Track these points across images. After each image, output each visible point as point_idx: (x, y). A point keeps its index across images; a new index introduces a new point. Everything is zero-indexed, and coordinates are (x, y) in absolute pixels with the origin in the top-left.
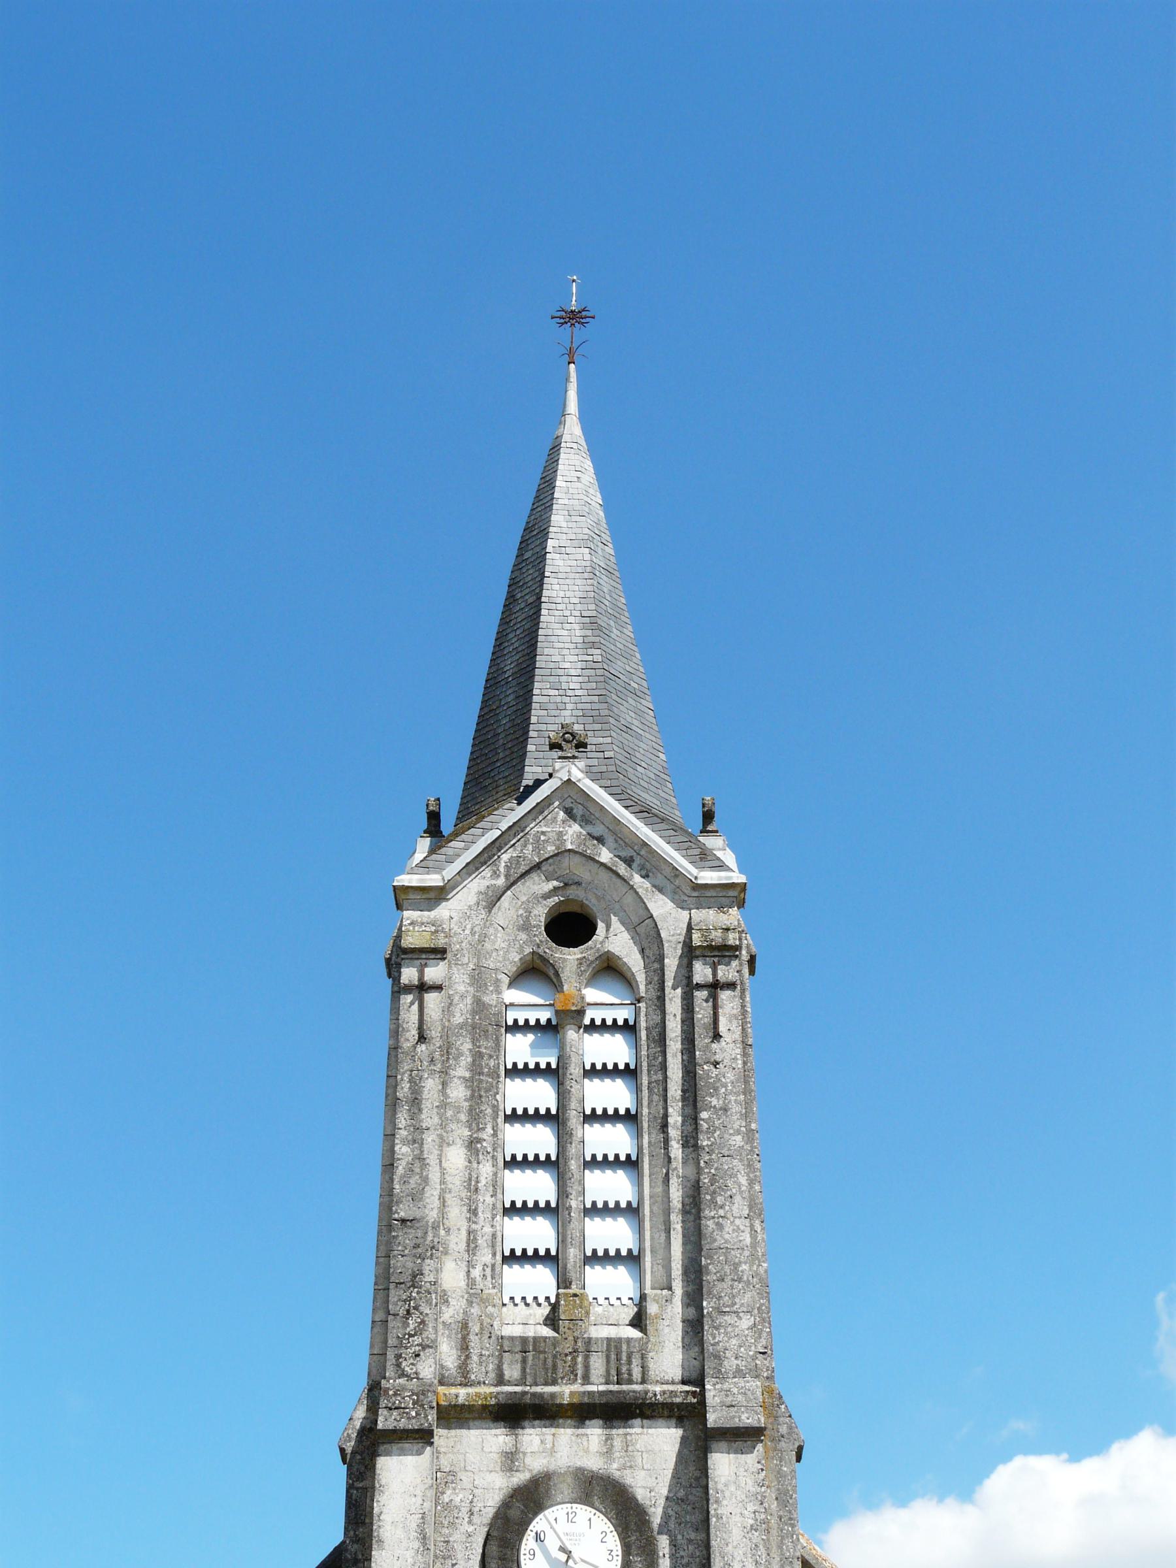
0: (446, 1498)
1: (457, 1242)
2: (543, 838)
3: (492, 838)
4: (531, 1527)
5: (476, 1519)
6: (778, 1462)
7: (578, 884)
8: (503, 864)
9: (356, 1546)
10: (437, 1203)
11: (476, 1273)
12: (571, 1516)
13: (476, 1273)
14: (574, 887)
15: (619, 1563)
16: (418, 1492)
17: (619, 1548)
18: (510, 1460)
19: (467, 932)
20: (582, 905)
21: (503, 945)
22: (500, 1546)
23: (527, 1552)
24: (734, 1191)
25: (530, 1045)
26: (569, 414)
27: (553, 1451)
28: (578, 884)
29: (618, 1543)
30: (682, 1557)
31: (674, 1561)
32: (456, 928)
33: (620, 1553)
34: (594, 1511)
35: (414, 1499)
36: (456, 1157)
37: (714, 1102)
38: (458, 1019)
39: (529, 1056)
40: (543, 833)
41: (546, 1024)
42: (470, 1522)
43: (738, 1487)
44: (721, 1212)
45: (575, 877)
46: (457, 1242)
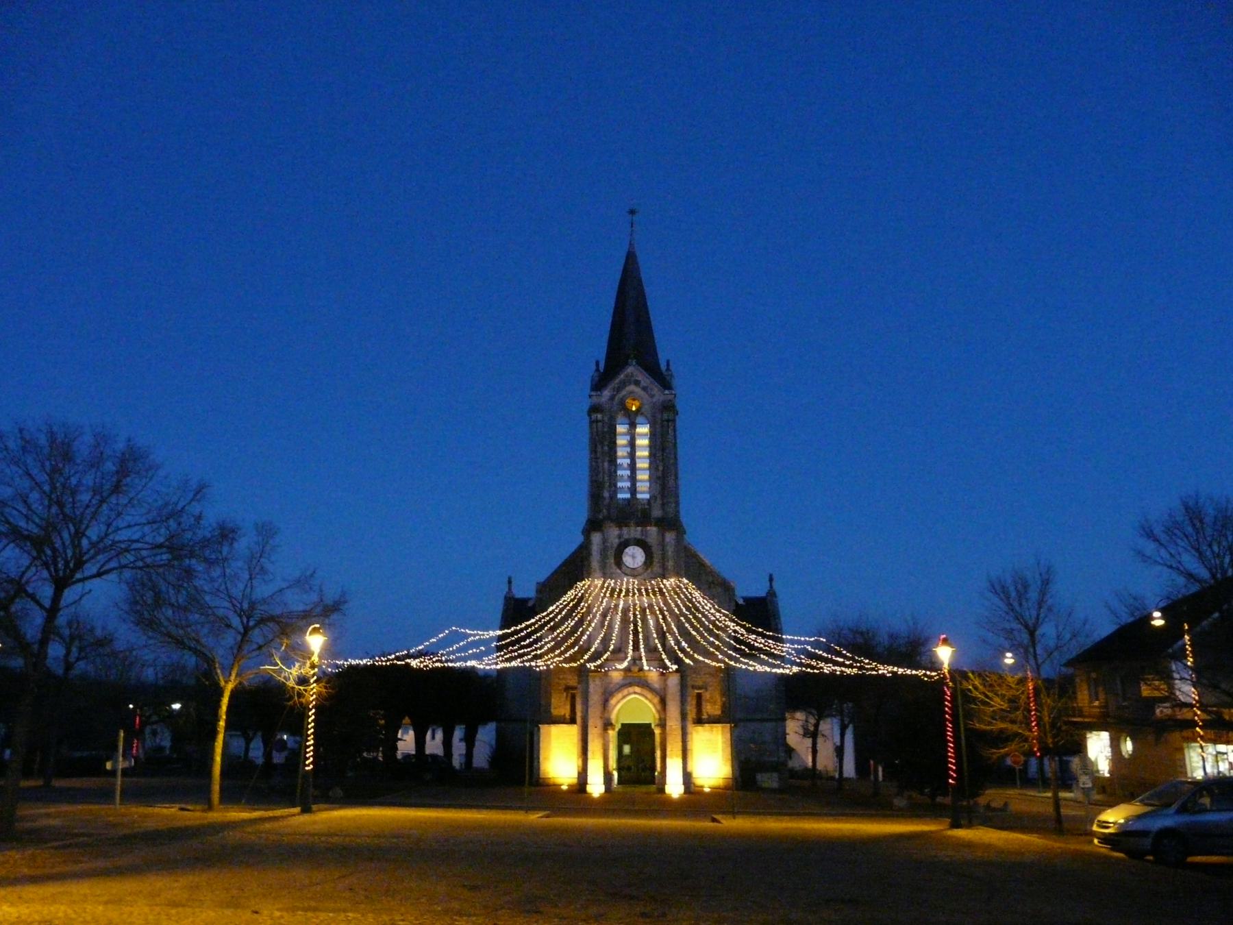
18: (620, 536)
27: (630, 535)
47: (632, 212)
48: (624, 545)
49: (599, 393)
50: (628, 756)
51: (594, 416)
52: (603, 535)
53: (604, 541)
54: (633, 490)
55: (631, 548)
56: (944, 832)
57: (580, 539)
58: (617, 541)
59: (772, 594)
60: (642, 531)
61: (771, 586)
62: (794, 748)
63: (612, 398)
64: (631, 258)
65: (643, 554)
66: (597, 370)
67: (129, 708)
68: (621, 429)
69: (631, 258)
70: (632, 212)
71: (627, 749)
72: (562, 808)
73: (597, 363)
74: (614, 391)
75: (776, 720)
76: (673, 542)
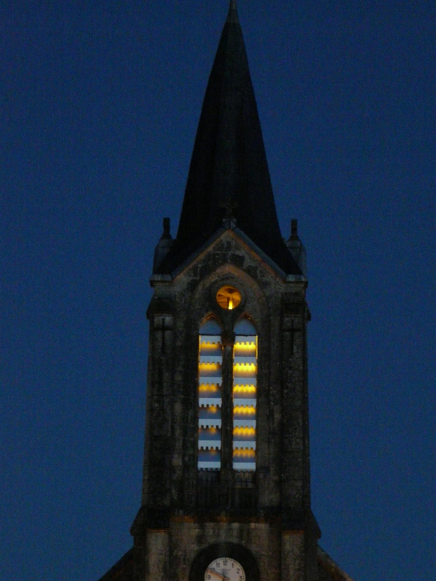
0: (174, 554)
1: (179, 444)
2: (217, 256)
6: (403, 185)
10: (170, 430)
11: (187, 459)
13: (187, 459)
15: (245, 580)
17: (244, 576)
18: (200, 539)
21: (199, 307)
22: (203, 260)
23: (207, 576)
24: (297, 426)
27: (218, 535)
28: (233, 278)
29: (244, 574)
31: (306, 367)
32: (177, 300)
33: (244, 577)
35: (161, 556)
36: (178, 408)
37: (290, 385)
38: (179, 344)
44: (291, 436)
46: (179, 444)
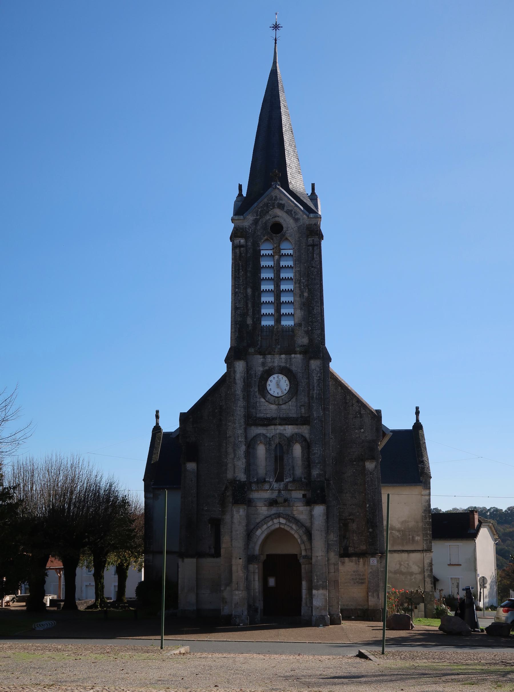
2: (269, 204)
3: (335, 627)
4: (269, 379)
5: (256, 377)
7: (278, 217)
8: (259, 212)
9: (229, 383)
12: (278, 377)
14: (277, 217)
16: (243, 372)
18: (263, 364)
19: (250, 231)
20: (279, 222)
25: (431, 477)
26: (276, 23)
28: (278, 217)
30: (303, 385)
34: (283, 376)
38: (249, 255)
39: (268, 553)
40: (269, 203)
41: (56, 607)
42: (255, 378)
43: (316, 371)
45: (277, 215)
47: (276, 27)
48: (269, 373)
49: (242, 217)
50: (131, 603)
51: (237, 241)
52: (247, 363)
53: (248, 369)
54: (278, 317)
55: (275, 376)
56: (295, 529)
57: (223, 369)
58: (261, 369)
59: (418, 426)
60: (286, 359)
61: (417, 420)
62: (468, 507)
63: (256, 222)
64: (274, 74)
65: (287, 382)
66: (240, 194)
67: (277, 582)
68: (266, 250)
69: (274, 74)
70: (276, 27)
71: (272, 582)
72: (177, 659)
73: (240, 187)
74: (257, 215)
75: (423, 551)
76: (318, 369)
